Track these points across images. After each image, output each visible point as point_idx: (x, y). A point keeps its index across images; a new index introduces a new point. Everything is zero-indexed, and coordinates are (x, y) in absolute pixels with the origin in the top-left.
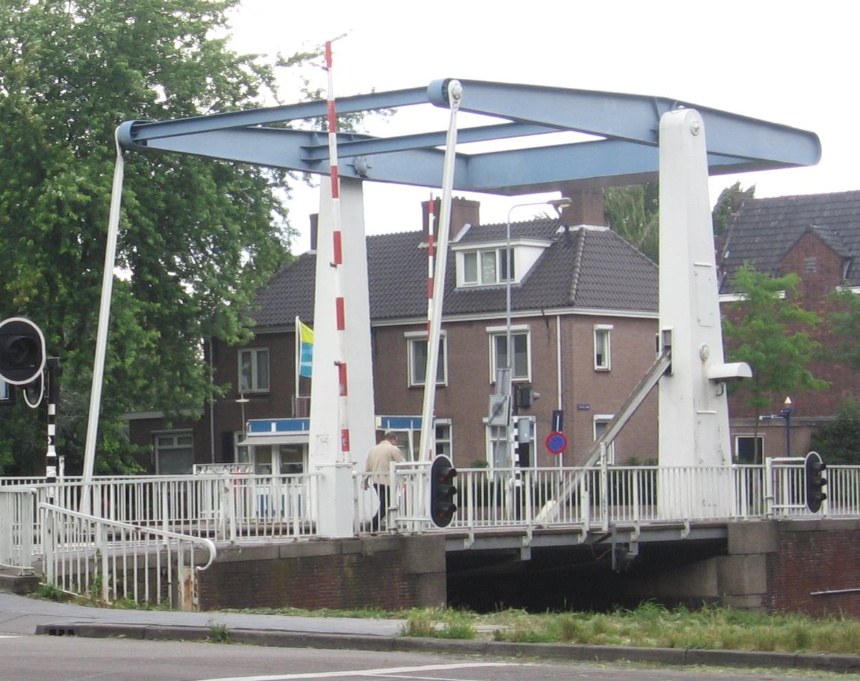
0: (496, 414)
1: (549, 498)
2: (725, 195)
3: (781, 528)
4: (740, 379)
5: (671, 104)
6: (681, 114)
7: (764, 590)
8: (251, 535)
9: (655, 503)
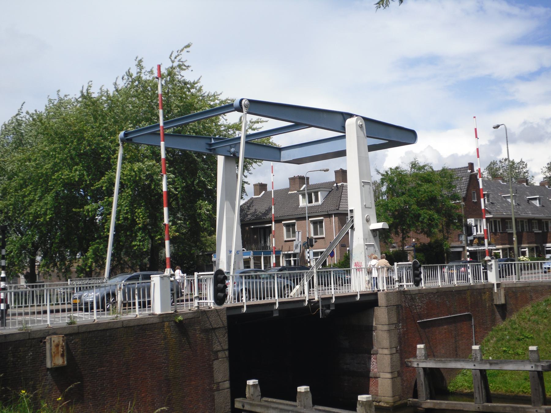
0: (296, 248)
1: (297, 284)
2: (452, 171)
3: (402, 293)
4: (383, 229)
5: (351, 116)
6: (354, 119)
7: (396, 322)
8: (68, 311)
9: (350, 283)
